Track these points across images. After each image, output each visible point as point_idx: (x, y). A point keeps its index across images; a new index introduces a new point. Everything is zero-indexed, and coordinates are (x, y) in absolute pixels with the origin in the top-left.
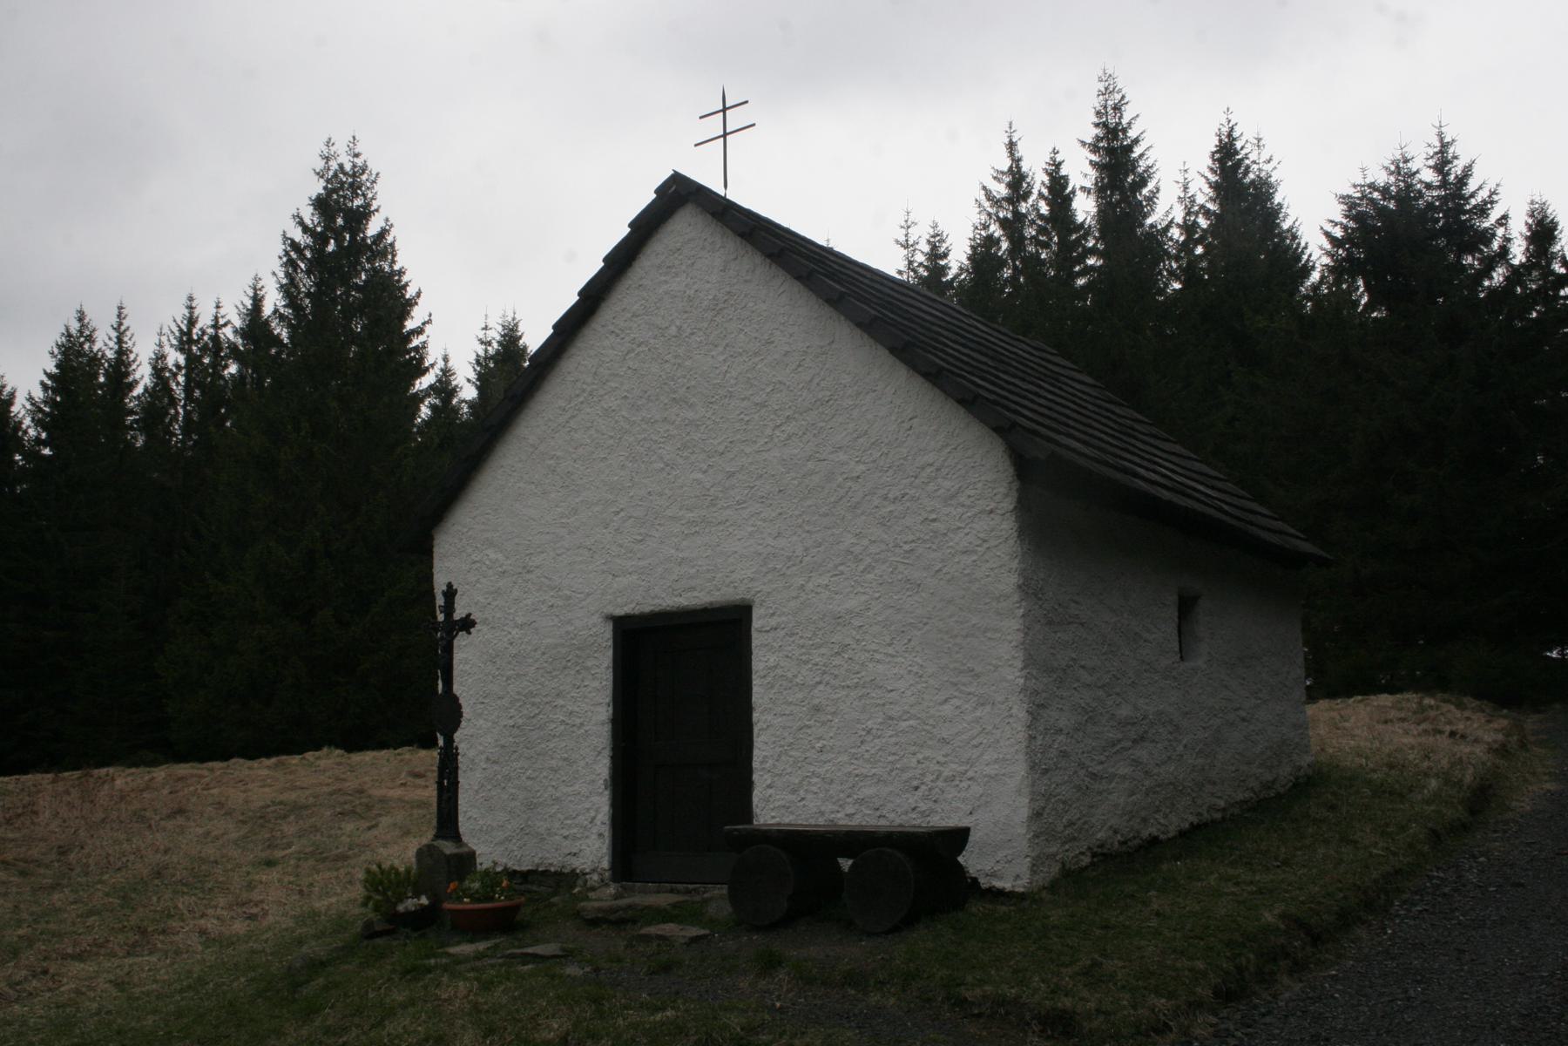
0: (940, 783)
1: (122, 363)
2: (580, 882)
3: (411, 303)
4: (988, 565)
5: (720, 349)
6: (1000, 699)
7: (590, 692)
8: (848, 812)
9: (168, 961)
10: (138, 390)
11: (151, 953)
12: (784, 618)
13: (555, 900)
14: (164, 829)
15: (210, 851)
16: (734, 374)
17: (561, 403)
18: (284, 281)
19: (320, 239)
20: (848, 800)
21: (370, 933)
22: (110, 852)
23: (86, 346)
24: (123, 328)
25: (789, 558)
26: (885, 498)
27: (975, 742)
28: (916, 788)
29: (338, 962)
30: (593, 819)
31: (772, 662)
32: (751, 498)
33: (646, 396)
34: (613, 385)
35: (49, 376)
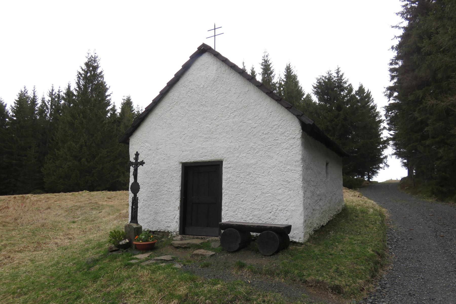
0: (277, 211)
1: (35, 99)
2: (170, 234)
3: (107, 89)
4: (293, 153)
5: (215, 91)
6: (296, 189)
7: (175, 183)
8: (250, 218)
9: (46, 253)
10: (38, 106)
11: (41, 250)
12: (232, 165)
13: (163, 239)
14: (45, 213)
15: (57, 219)
16: (219, 98)
17: (168, 105)
18: (77, 81)
19: (86, 72)
20: (250, 215)
21: (111, 251)
22: (29, 219)
23: (26, 94)
24: (35, 91)
25: (234, 149)
26: (263, 133)
27: (288, 201)
28: (270, 213)
29: (102, 259)
30: (175, 217)
31: (228, 177)
32: (223, 132)
33: (193, 103)
34: (184, 100)
35: (16, 101)
